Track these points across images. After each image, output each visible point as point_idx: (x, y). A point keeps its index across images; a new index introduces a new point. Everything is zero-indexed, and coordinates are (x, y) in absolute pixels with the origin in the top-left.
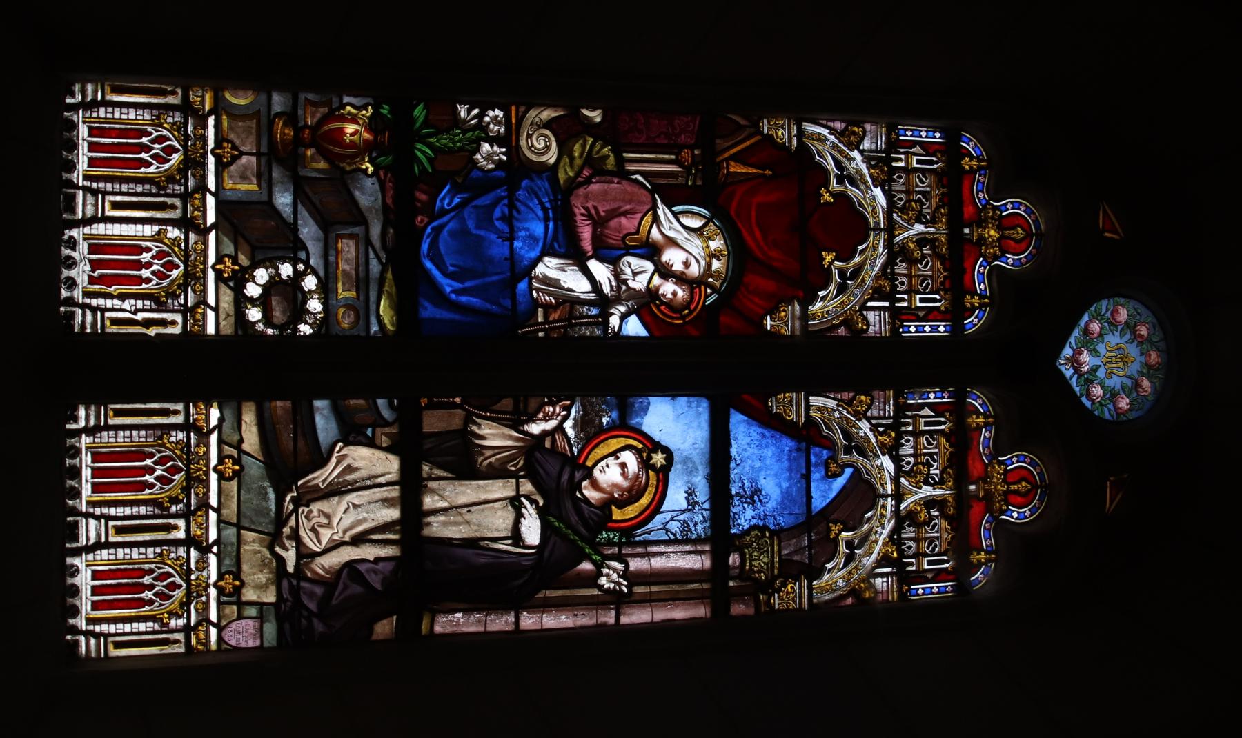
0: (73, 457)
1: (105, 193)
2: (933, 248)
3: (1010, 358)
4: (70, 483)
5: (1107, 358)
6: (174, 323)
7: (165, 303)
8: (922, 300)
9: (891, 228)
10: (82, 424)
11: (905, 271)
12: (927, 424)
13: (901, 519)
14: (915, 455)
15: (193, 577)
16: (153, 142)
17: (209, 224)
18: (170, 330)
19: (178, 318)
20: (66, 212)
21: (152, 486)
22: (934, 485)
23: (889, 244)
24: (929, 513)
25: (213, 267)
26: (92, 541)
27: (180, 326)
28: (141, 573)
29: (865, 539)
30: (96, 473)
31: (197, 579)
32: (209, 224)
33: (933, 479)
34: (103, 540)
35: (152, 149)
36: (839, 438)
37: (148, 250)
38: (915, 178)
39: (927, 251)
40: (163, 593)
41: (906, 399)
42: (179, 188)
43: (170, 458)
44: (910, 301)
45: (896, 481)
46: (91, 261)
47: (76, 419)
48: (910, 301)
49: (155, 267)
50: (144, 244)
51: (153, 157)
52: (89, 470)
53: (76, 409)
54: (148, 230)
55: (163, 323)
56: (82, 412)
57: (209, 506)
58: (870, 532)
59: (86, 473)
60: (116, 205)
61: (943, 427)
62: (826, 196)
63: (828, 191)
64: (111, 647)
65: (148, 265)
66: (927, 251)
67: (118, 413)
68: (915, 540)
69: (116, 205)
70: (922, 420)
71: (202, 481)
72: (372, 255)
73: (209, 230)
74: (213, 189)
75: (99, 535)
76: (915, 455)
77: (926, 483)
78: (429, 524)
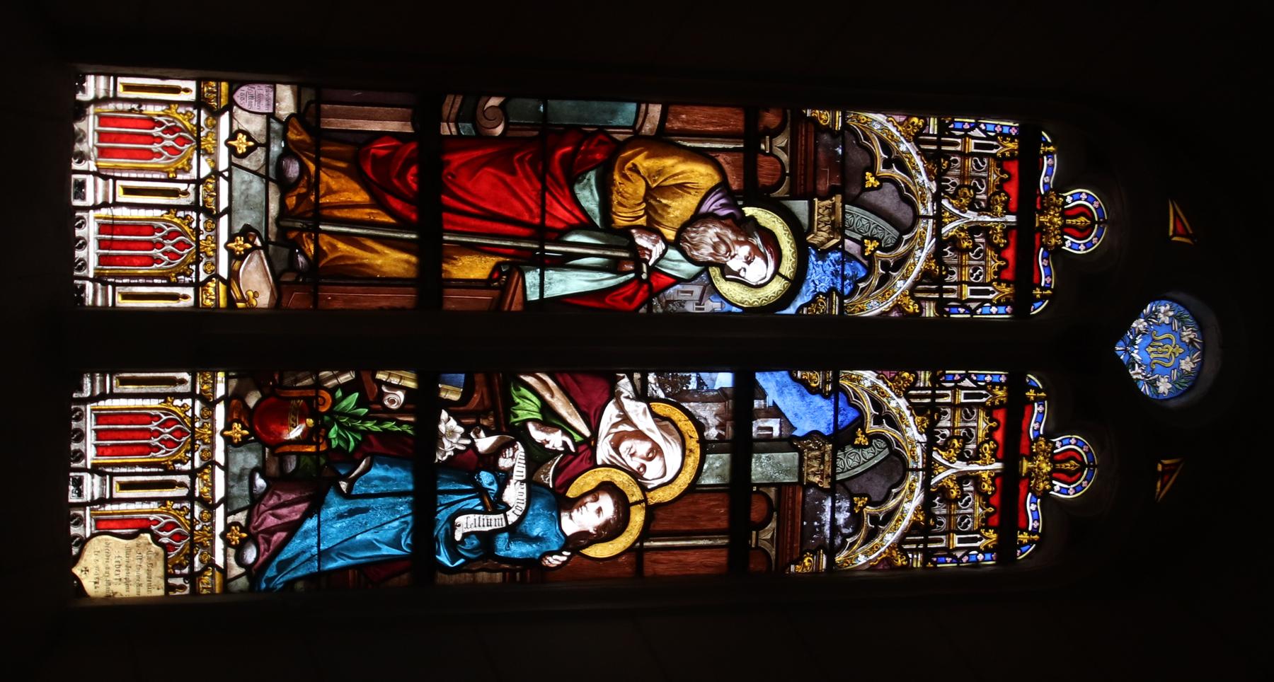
0: (78, 440)
1: (115, 179)
2: (989, 239)
3: (1061, 348)
4: (74, 446)
5: (1161, 351)
6: (185, 297)
7: (173, 279)
8: (960, 541)
9: (930, 468)
10: (87, 393)
11: (944, 511)
12: (967, 396)
13: (941, 243)
14: (962, 177)
15: (202, 237)
16: (164, 237)
17: (222, 506)
18: (182, 303)
19: (190, 291)
20: (75, 198)
21: (159, 261)
22: (981, 211)
23: (926, 485)
24: (961, 488)
25: (222, 434)
26: (100, 201)
27: (189, 385)
28: (148, 419)
29: (890, 515)
30: (100, 434)
31: (202, 529)
32: (222, 506)
33: (968, 453)
34: (111, 95)
35: (163, 245)
36: (869, 409)
37: (161, 230)
38: (969, 162)
39: (980, 239)
40: (172, 252)
41: (949, 313)
42: (188, 467)
43: (175, 525)
44: (954, 397)
45: (928, 452)
46: (99, 148)
47: (81, 390)
48: (954, 397)
49: (166, 143)
50: (152, 412)
51: (161, 441)
52: (93, 434)
53: (81, 378)
54: (154, 403)
55: (175, 297)
56: (87, 381)
57: (215, 463)
58: (896, 508)
59: (91, 437)
60: (128, 191)
61: (994, 151)
62: (872, 180)
63: (874, 175)
64: (118, 298)
65: (157, 433)
66: (969, 487)
67: (124, 382)
68: (948, 516)
69: (124, 486)
70: (973, 142)
71: (205, 547)
72: (387, 219)
73: (220, 215)
74: (222, 462)
75: (106, 195)
76: (962, 177)
77: (972, 208)
78: (449, 162)
